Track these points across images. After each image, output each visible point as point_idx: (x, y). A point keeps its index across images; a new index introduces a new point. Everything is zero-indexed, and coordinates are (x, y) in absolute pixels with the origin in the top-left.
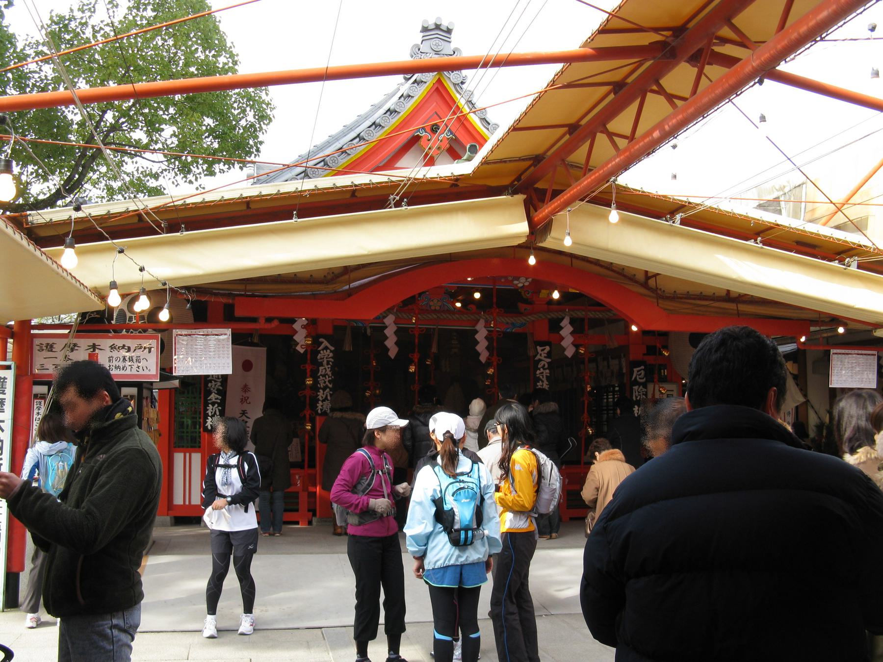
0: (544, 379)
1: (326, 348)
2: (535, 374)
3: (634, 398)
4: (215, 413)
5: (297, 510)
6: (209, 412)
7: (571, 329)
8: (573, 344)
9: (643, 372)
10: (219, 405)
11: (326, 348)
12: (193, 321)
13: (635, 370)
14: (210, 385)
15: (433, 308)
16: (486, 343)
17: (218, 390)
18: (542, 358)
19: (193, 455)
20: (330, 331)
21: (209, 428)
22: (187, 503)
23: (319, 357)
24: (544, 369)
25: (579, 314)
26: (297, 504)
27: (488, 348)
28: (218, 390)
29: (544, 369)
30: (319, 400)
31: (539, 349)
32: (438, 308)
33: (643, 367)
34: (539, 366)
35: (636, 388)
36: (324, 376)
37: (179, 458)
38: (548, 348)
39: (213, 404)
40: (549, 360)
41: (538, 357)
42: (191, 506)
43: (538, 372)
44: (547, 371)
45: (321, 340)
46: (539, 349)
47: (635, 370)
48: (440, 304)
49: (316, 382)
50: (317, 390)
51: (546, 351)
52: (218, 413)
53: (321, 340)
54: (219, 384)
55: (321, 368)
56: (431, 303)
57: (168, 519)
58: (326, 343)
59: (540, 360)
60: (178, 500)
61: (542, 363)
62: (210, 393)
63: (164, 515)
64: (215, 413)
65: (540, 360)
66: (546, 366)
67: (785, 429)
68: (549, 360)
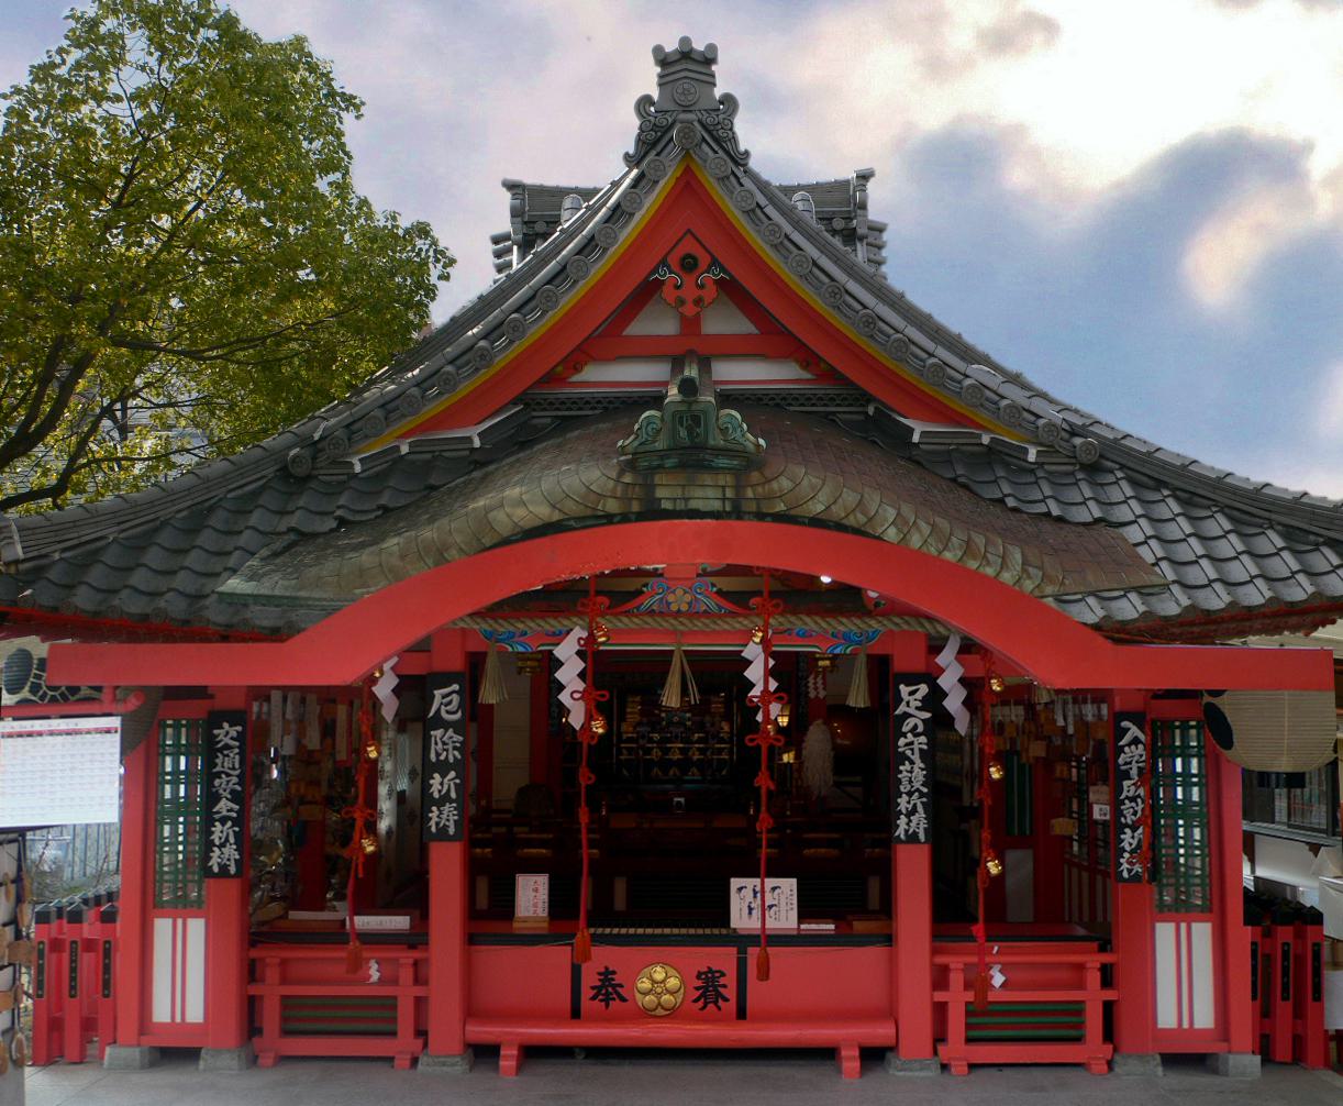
0: (916, 758)
1: (1136, 741)
4: (227, 840)
5: (393, 1034)
6: (216, 838)
8: (961, 680)
9: (455, 698)
10: (235, 822)
11: (1136, 741)
13: (438, 693)
15: (674, 608)
16: (961, 694)
17: (233, 792)
18: (911, 711)
21: (216, 869)
22: (178, 1019)
23: (1121, 761)
26: (394, 1020)
28: (233, 792)
31: (904, 690)
32: (684, 608)
33: (456, 687)
34: (905, 729)
35: (437, 733)
36: (1133, 799)
37: (162, 927)
38: (923, 689)
39: (223, 821)
41: (902, 709)
42: (185, 1027)
43: (902, 741)
44: (923, 739)
45: (1125, 724)
46: (904, 690)
47: (438, 693)
48: (688, 598)
49: (1117, 812)
50: (1121, 828)
51: (919, 695)
52: (232, 840)
53: (1125, 724)
54: (235, 780)
55: (1126, 783)
56: (671, 598)
58: (1134, 731)
59: (907, 716)
60: (161, 1012)
61: (911, 722)
62: (218, 798)
63: (131, 1046)
64: (227, 840)
65: (907, 716)
66: (920, 729)
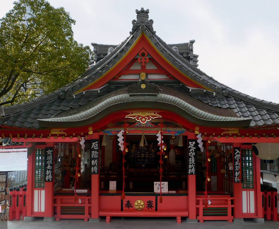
1: (238, 153)
3: (92, 157)
4: (49, 174)
5: (84, 214)
8: (202, 141)
9: (97, 144)
11: (238, 153)
13: (93, 143)
14: (47, 162)
16: (202, 144)
17: (51, 164)
18: (192, 147)
19: (42, 191)
20: (239, 146)
21: (47, 180)
23: (235, 158)
27: (203, 146)
28: (51, 164)
29: (193, 152)
33: (97, 142)
34: (190, 151)
35: (93, 152)
36: (238, 165)
37: (36, 192)
38: (194, 143)
39: (49, 170)
41: (190, 147)
43: (190, 154)
44: (194, 153)
45: (236, 150)
51: (193, 144)
52: (50, 174)
53: (236, 150)
54: (51, 161)
55: (236, 162)
57: (30, 218)
58: (238, 151)
59: (191, 148)
60: (36, 210)
61: (191, 150)
62: (47, 165)
64: (49, 174)
65: (191, 148)
66: (194, 151)
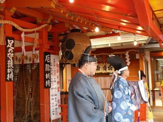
0: (11, 59)
2: (6, 55)
3: (46, 70)
7: (129, 56)
12: (34, 34)
13: (47, 56)
24: (11, 53)
25: (33, 30)
29: (11, 53)
30: (8, 73)
31: (9, 41)
35: (46, 65)
40: (13, 48)
43: (8, 54)
44: (12, 54)
46: (9, 41)
47: (47, 56)
61: (10, 50)
66: (12, 52)
67: (130, 80)
68: (13, 48)
